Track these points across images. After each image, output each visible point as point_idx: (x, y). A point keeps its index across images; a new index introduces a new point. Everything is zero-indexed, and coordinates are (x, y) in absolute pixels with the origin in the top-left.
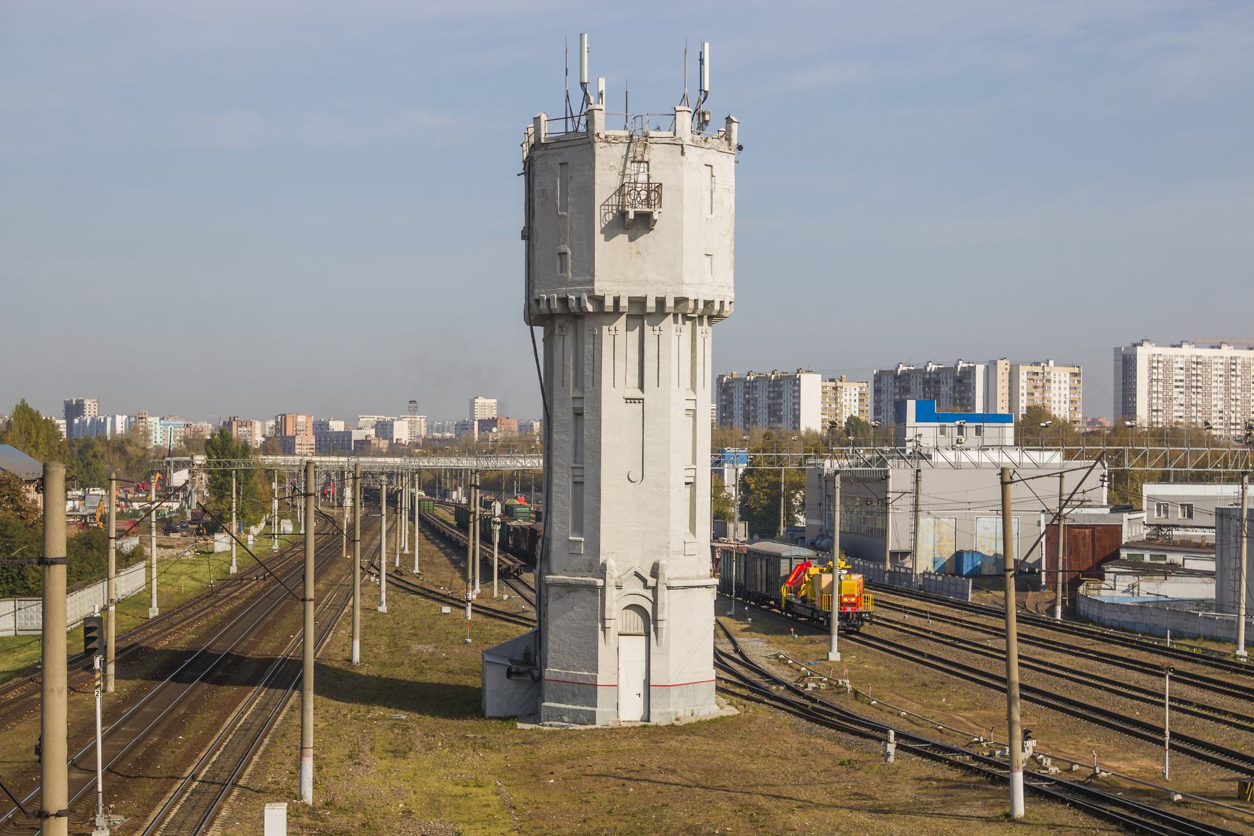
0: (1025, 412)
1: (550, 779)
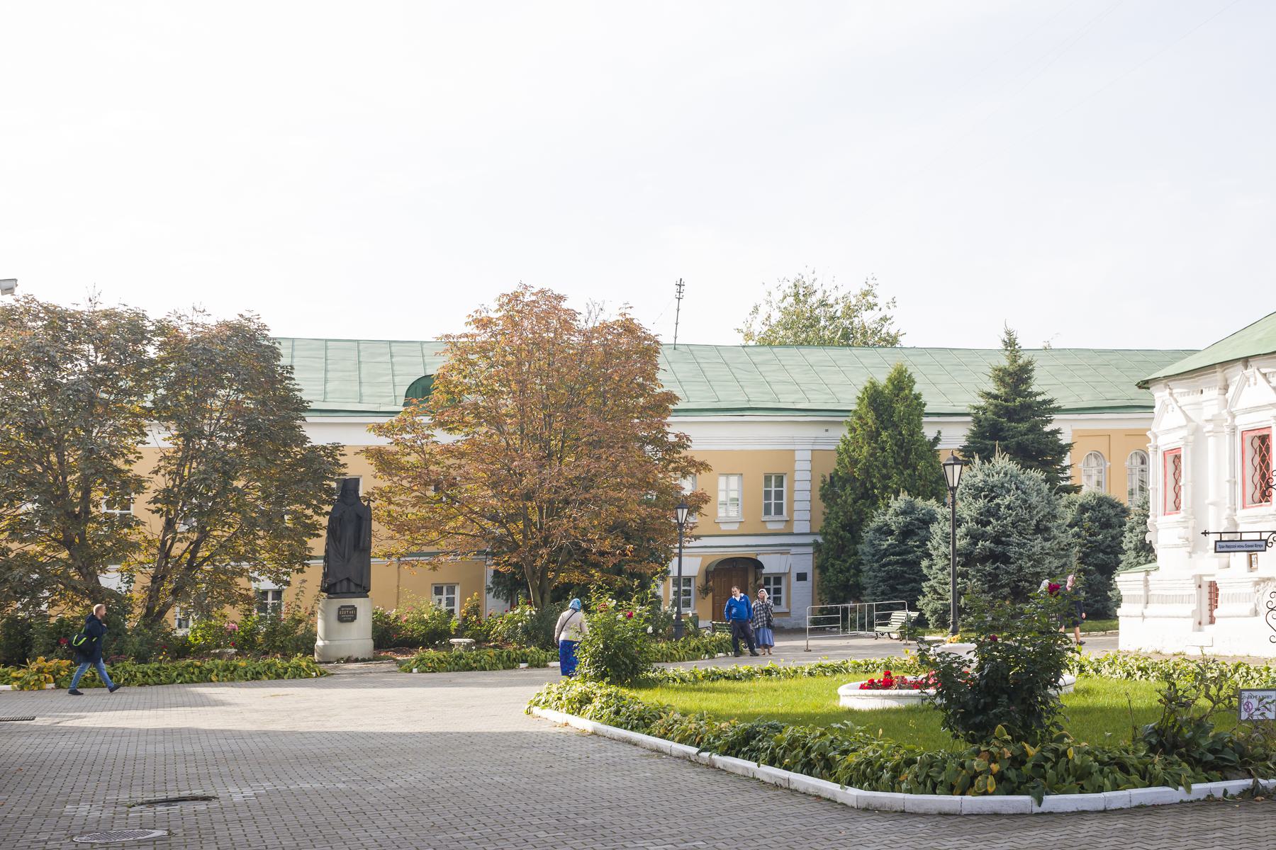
0: (1061, 750)
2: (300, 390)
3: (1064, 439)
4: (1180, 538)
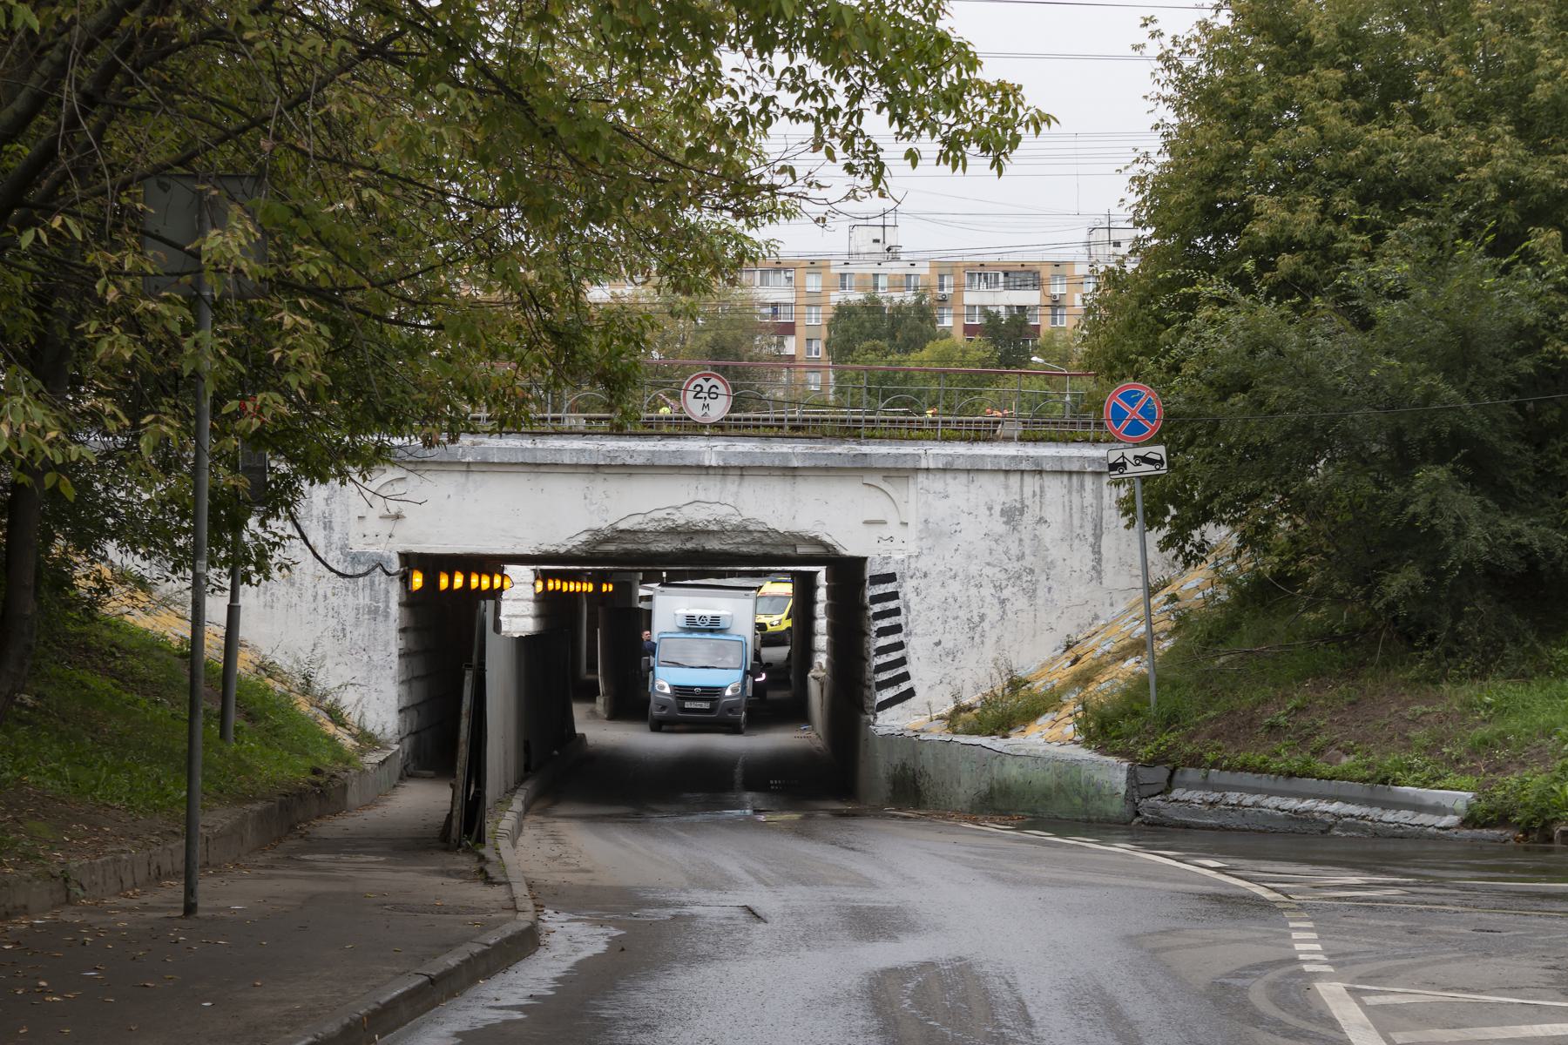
2: (964, 169)
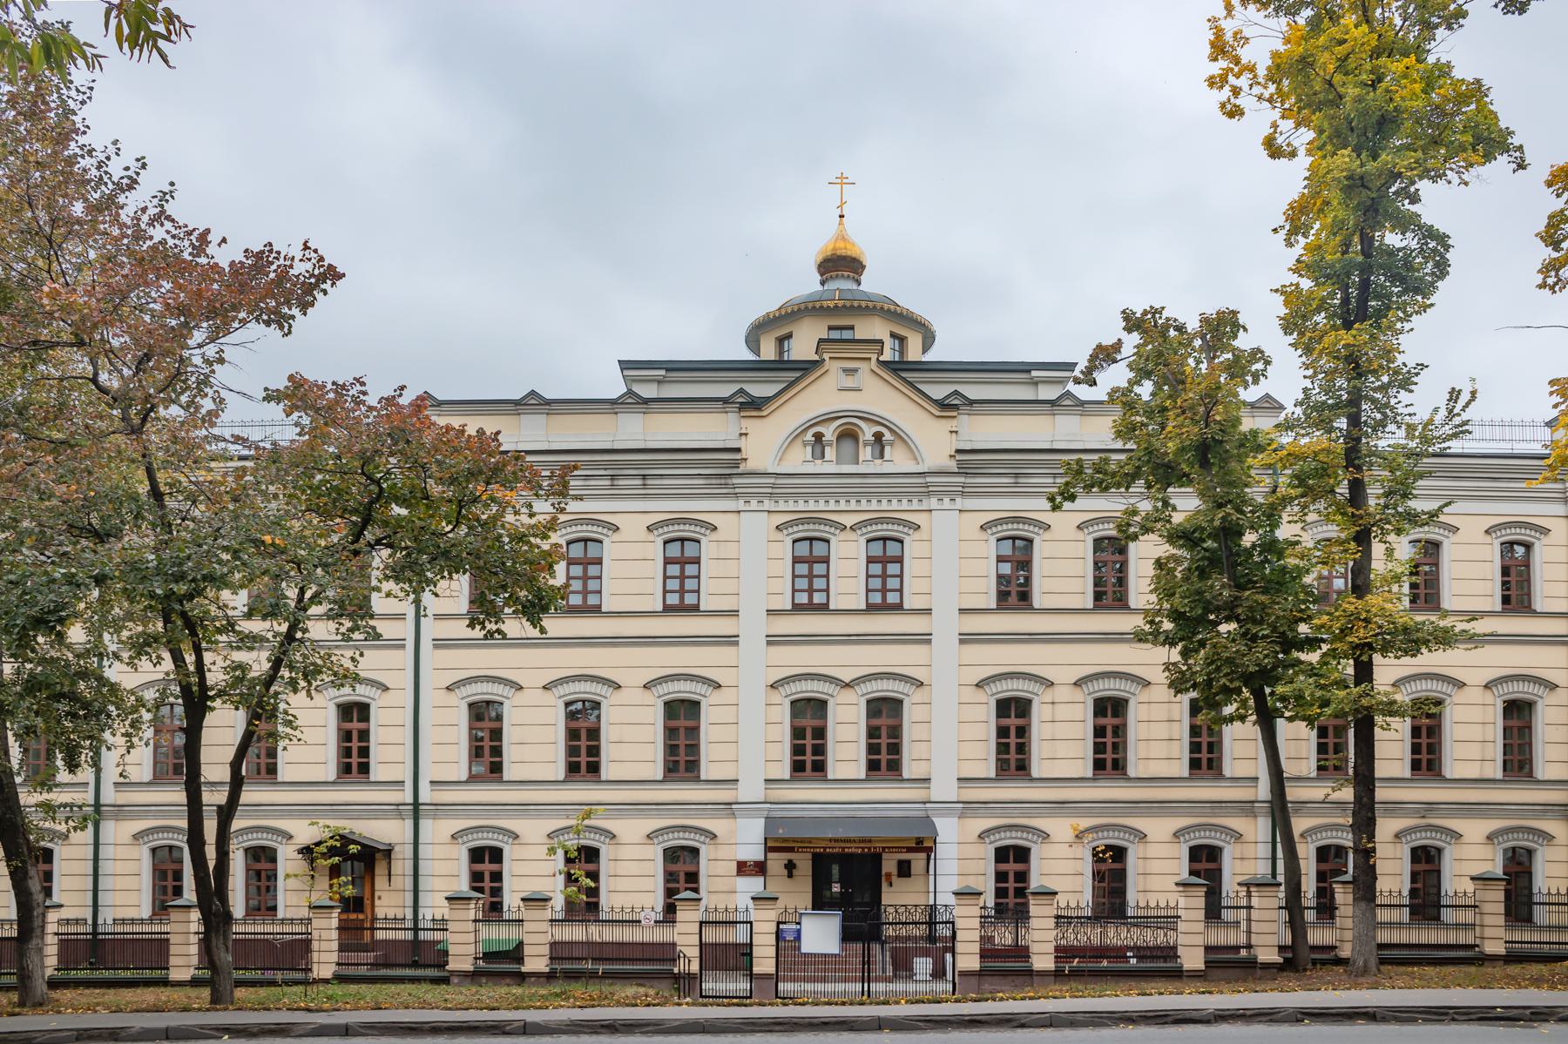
1: (1183, 364)
3: (1303, 130)
4: (121, 49)
